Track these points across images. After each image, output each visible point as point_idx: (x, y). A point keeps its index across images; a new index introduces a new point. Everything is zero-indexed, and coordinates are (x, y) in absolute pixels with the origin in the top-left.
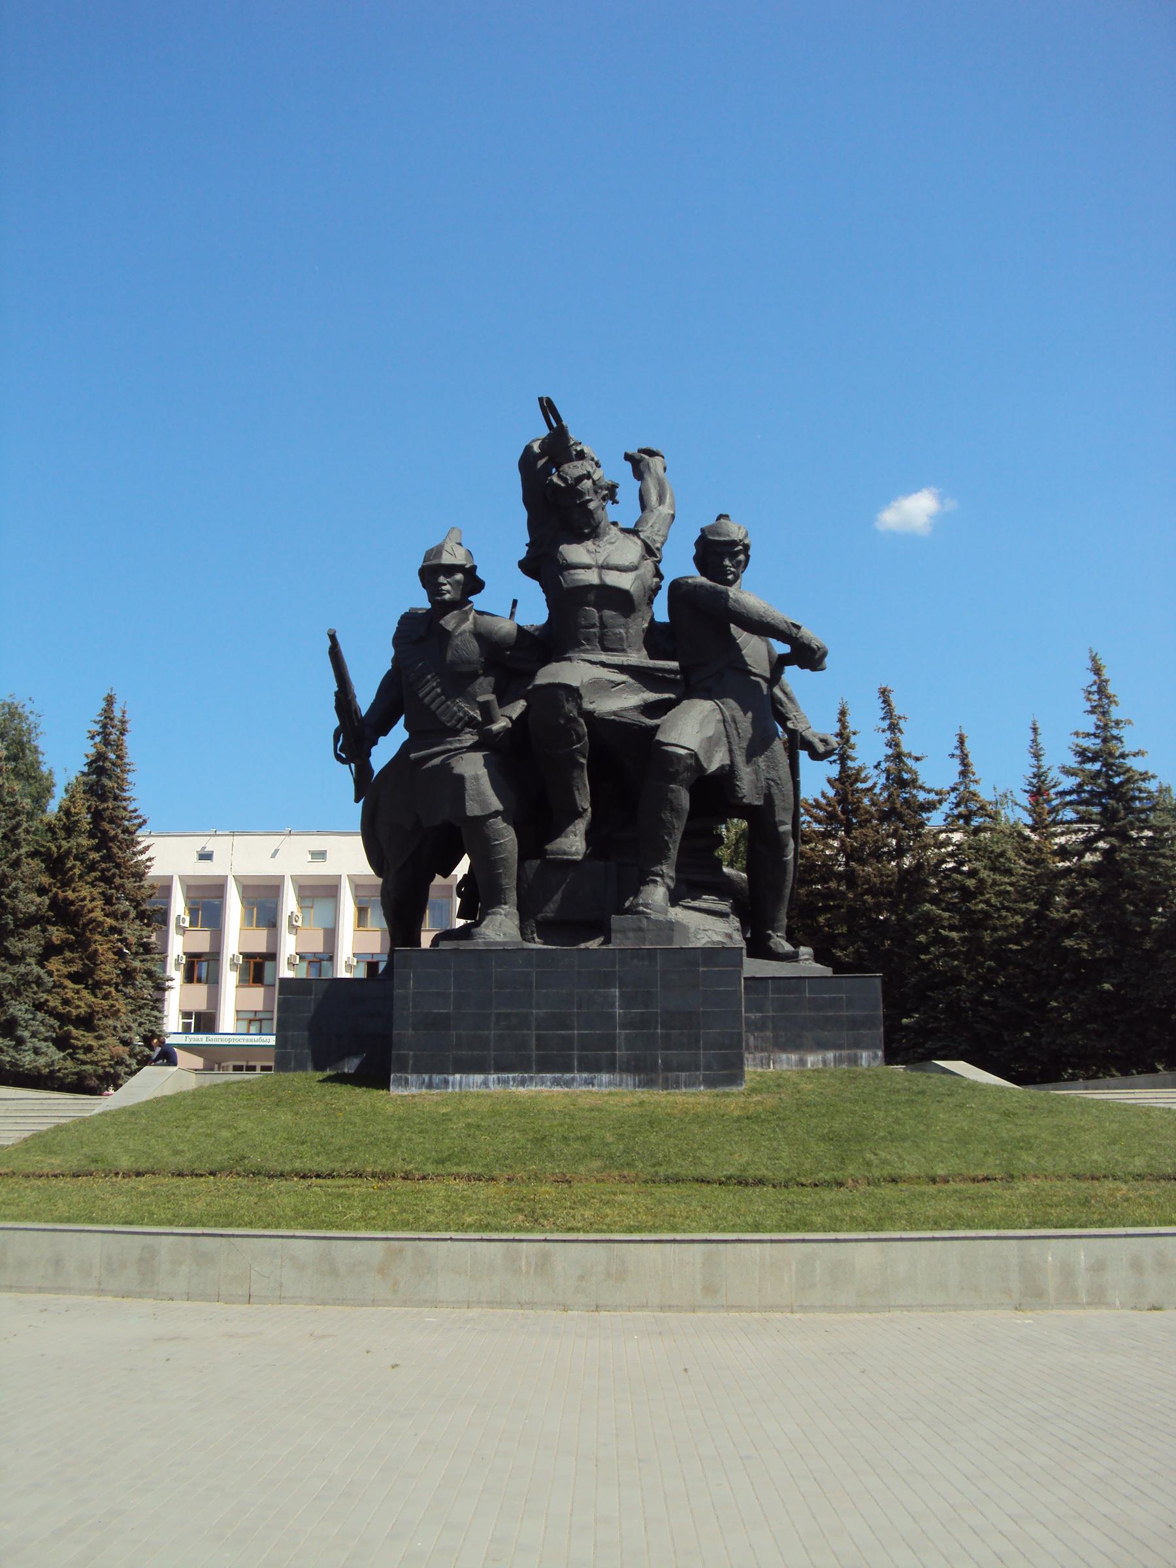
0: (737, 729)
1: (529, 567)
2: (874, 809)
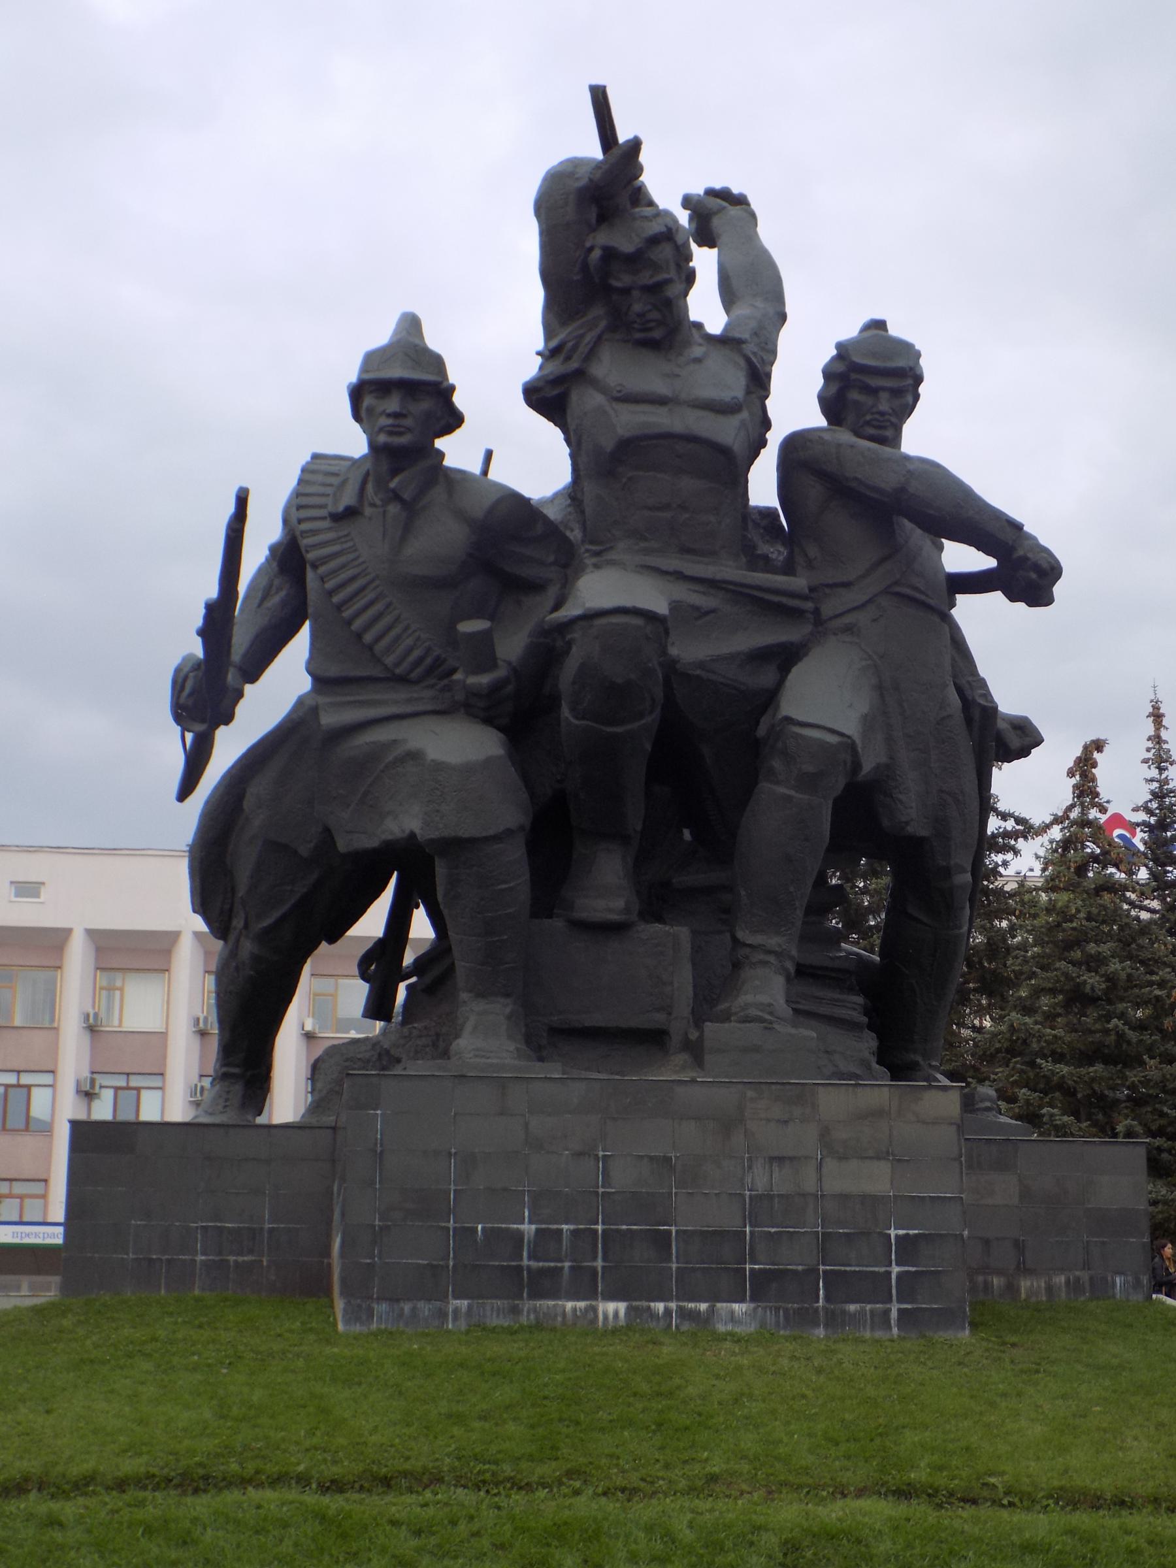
1: (546, 397)
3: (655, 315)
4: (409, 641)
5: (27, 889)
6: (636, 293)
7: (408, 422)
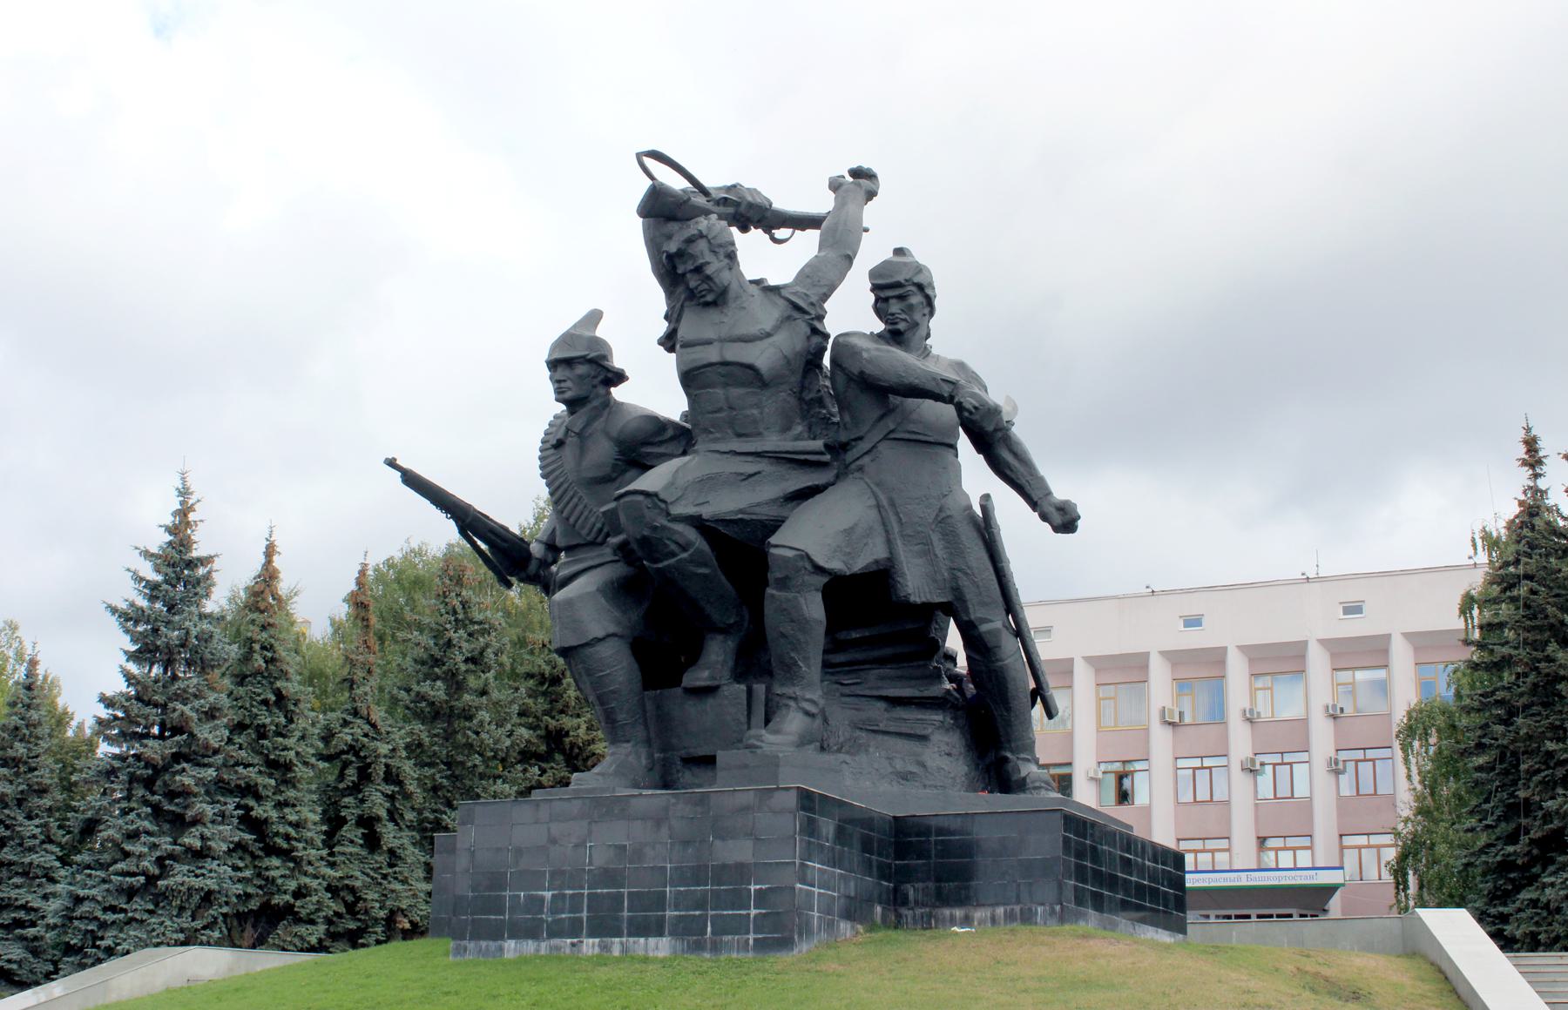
0: (897, 514)
2: (158, 605)
3: (705, 286)
7: (569, 384)
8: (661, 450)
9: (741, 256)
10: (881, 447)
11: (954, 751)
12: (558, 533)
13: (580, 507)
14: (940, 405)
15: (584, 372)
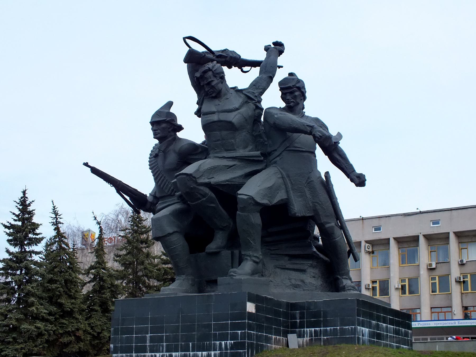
3: (212, 90)
4: (170, 186)
5: (378, 229)
6: (205, 86)
7: (159, 131)
8: (197, 157)
9: (227, 78)
10: (283, 154)
11: (316, 276)
12: (157, 192)
13: (165, 181)
14: (307, 136)
15: (165, 124)
